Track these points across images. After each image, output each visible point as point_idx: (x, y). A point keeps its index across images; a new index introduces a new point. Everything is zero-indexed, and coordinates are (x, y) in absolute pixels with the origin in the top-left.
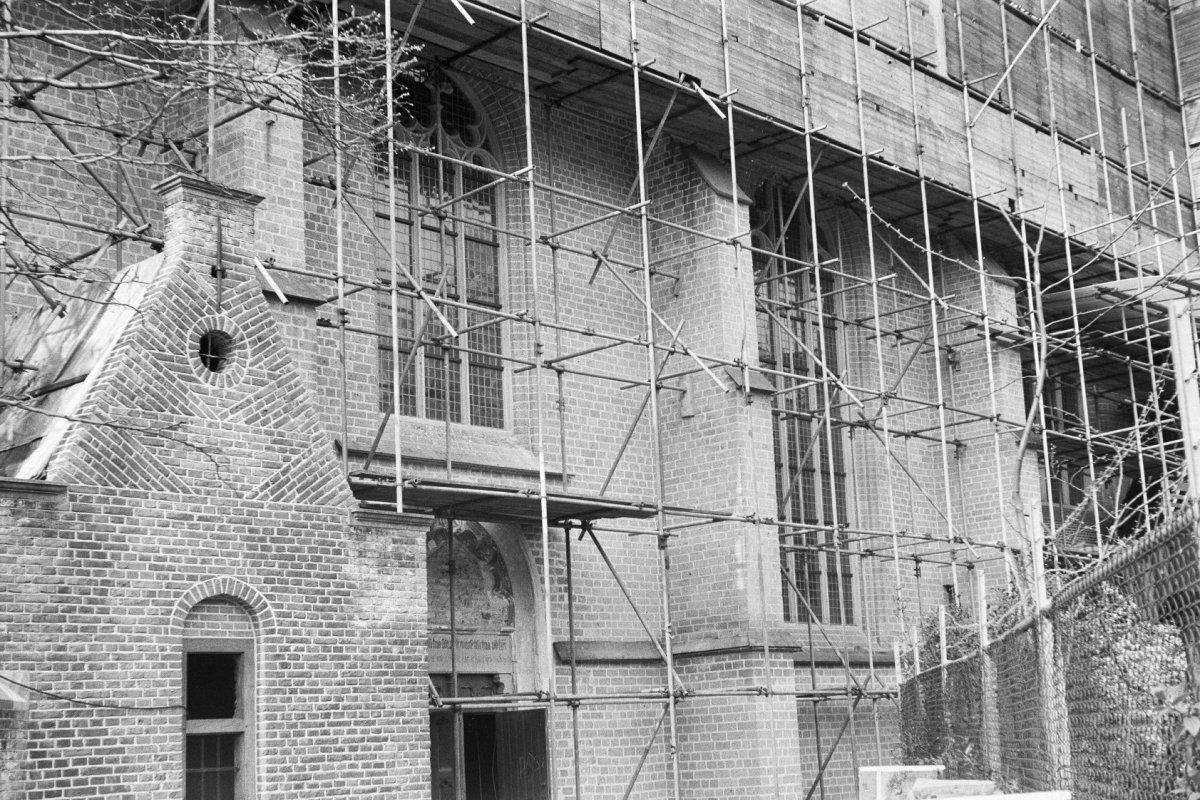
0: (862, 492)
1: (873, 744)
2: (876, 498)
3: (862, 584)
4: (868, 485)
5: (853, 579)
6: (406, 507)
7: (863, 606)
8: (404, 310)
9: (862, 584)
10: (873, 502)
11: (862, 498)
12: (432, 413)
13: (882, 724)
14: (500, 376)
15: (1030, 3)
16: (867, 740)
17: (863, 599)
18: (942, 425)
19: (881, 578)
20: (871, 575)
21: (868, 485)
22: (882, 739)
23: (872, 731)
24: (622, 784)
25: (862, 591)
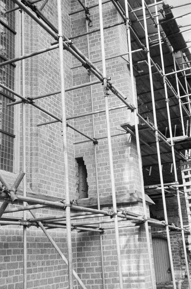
0: (26, 79)
1: (21, 269)
2: (36, 85)
3: (22, 143)
4: (31, 75)
5: (15, 140)
6: (166, 236)
7: (21, 159)
8: (71, 154)
9: (22, 143)
10: (34, 87)
11: (27, 83)
12: (118, 204)
13: (29, 252)
14: (14, 70)
15: (84, 2)
16: (14, 266)
17: (21, 154)
18: (63, 90)
19: (37, 140)
20: (29, 137)
21: (31, 75)
22: (29, 265)
23: (20, 258)
24: (49, 90)
25: (22, 148)
